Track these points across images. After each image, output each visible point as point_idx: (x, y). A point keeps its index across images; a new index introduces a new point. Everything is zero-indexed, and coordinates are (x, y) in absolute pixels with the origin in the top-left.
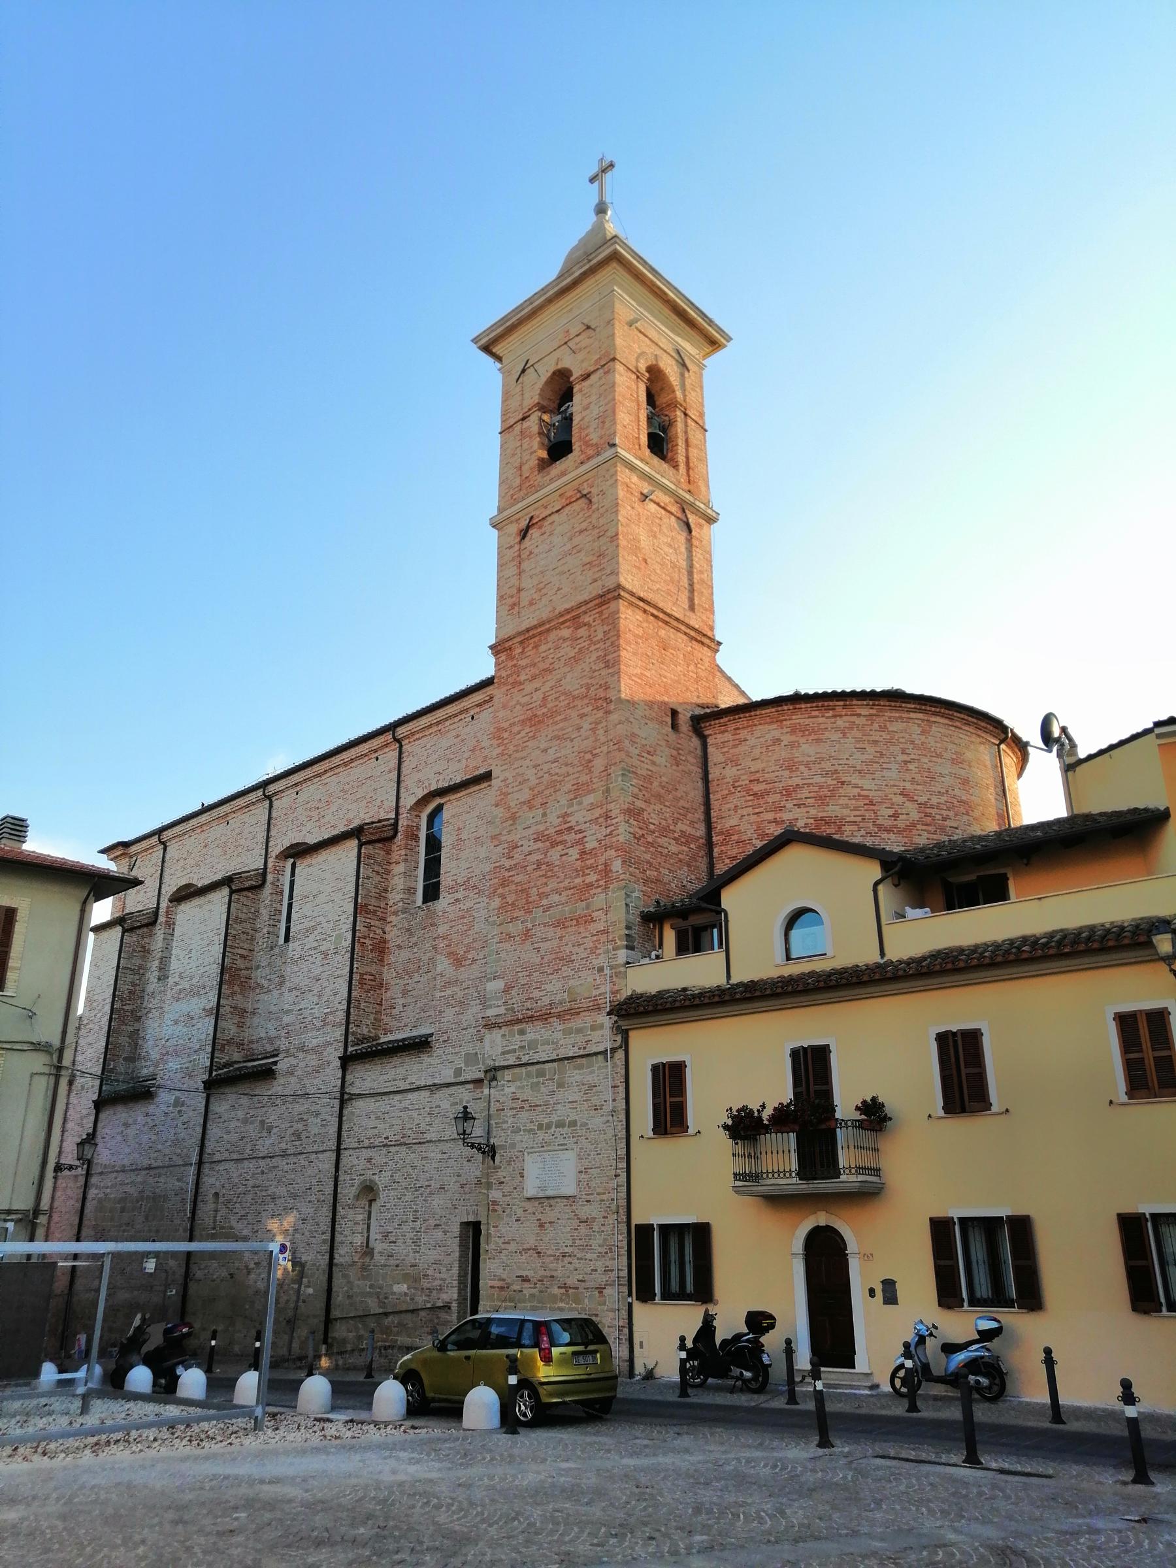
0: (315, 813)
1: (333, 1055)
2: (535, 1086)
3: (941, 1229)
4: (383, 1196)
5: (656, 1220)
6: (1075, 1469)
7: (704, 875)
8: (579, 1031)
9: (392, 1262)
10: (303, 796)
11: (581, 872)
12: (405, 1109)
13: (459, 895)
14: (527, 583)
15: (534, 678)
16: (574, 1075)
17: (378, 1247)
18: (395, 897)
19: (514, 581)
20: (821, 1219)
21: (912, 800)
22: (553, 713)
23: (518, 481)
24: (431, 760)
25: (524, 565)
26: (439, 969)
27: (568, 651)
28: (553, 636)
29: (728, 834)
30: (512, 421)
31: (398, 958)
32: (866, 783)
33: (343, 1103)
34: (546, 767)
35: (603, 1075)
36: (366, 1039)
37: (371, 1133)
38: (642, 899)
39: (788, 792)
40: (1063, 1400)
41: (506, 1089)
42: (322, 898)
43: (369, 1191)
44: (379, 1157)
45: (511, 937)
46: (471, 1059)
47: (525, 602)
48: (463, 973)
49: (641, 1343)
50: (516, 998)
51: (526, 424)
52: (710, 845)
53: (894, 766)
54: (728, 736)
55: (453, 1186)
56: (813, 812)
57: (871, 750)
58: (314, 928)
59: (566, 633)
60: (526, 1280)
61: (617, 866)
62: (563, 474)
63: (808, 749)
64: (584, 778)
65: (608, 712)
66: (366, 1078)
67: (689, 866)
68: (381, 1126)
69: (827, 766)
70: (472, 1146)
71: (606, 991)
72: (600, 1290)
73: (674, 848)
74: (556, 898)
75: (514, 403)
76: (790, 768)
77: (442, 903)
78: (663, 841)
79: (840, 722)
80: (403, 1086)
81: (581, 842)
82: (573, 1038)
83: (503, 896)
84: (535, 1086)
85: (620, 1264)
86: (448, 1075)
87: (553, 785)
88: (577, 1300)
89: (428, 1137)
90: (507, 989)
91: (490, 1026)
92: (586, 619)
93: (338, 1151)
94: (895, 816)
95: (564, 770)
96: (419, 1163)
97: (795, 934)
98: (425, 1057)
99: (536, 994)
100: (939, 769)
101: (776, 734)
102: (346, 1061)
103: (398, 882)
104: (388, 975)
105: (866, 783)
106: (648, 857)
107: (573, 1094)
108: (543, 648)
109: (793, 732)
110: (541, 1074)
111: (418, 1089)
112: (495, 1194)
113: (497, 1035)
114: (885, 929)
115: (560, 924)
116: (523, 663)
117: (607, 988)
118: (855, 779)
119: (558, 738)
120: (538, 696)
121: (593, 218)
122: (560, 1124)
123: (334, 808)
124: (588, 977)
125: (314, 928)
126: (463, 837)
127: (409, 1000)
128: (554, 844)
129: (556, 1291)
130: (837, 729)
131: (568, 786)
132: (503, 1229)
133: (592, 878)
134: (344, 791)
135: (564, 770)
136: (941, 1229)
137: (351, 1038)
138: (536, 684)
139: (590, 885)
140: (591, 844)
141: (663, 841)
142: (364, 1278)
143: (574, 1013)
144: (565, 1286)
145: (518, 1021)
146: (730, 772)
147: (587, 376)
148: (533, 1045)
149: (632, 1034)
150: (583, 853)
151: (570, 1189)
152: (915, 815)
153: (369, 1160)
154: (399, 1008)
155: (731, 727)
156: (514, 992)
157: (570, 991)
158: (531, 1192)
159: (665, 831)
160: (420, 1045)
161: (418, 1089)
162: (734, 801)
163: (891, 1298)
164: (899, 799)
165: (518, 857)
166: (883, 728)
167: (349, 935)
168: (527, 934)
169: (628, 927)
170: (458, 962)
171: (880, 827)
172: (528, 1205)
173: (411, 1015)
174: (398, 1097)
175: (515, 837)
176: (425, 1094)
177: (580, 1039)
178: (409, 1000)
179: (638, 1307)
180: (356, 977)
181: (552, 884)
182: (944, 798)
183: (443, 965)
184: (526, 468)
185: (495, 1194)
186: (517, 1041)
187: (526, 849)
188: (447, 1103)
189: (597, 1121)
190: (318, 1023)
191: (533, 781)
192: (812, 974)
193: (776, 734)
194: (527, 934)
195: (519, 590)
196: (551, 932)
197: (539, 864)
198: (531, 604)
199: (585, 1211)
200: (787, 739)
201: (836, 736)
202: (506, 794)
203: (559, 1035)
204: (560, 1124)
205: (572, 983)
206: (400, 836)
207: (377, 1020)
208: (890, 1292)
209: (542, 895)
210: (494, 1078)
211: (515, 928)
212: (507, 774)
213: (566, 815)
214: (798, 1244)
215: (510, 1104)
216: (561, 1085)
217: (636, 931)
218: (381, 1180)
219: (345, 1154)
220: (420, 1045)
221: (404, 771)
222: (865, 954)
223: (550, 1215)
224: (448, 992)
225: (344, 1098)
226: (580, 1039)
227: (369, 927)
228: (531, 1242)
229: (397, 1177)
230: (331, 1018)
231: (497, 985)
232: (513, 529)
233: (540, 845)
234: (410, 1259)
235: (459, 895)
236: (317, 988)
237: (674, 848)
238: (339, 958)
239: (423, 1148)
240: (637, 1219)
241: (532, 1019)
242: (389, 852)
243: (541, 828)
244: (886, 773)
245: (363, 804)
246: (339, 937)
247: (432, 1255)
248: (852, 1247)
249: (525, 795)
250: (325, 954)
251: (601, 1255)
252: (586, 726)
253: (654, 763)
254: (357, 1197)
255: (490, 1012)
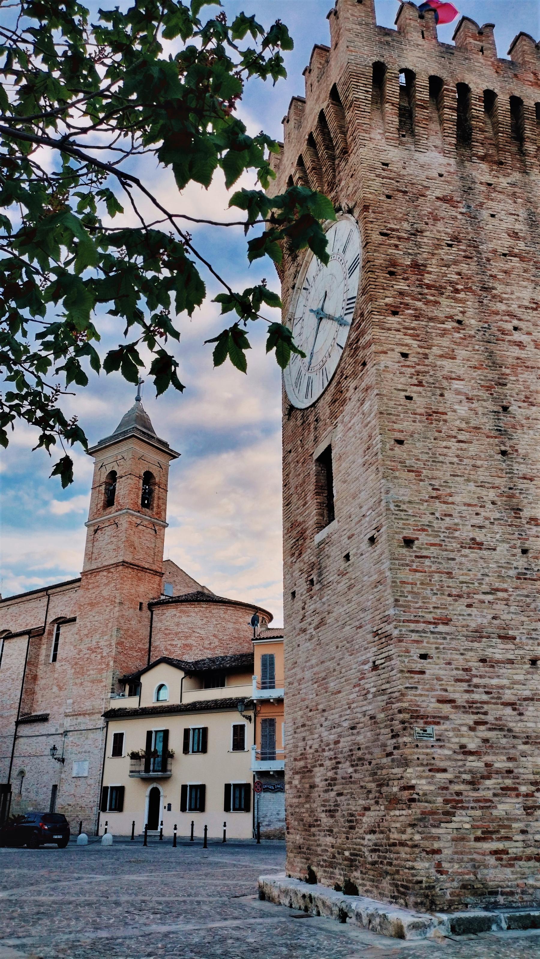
0: (14, 618)
1: (14, 719)
2: (79, 738)
3: (184, 787)
4: (27, 775)
5: (110, 785)
6: (247, 858)
7: (146, 663)
8: (94, 720)
9: (28, 799)
10: (10, 611)
11: (100, 664)
12: (37, 743)
13: (63, 663)
14: (95, 551)
15: (93, 588)
16: (91, 735)
17: (24, 794)
18: (42, 658)
19: (91, 549)
20: (154, 785)
21: (216, 637)
22: (98, 603)
23: (95, 511)
24: (60, 605)
25: (95, 543)
26: (54, 690)
27: (105, 581)
28: (101, 574)
29: (156, 647)
30: (96, 485)
31: (41, 682)
32: (202, 632)
33: (15, 739)
34: (94, 623)
35: (99, 736)
36: (27, 714)
37: (24, 751)
38: (120, 674)
39: (177, 634)
40: (208, 836)
41: (71, 738)
42: (14, 657)
43: (22, 773)
44: (27, 761)
45: (76, 684)
46: (62, 725)
47: (93, 558)
48: (62, 693)
49: (162, 822)
50: (76, 707)
51: (101, 488)
52: (150, 651)
53: (212, 626)
54: (160, 612)
55: (51, 772)
56: (183, 642)
57: (205, 620)
58: (10, 668)
59: (105, 573)
60: (69, 805)
61: (112, 663)
62: (110, 513)
63: (184, 619)
64: (105, 629)
65: (115, 607)
66: (25, 730)
67: (140, 660)
68: (28, 748)
69: (190, 625)
70: (55, 759)
71: (104, 707)
72: (91, 808)
73: (135, 654)
74: (92, 672)
75: (97, 479)
76: (177, 625)
77: (57, 664)
78: (130, 652)
79: (196, 609)
80: (37, 734)
81: (101, 653)
82: (92, 722)
83: (75, 669)
84: (79, 738)
85: (97, 800)
86: (53, 731)
87: (96, 630)
88: (84, 811)
89: (45, 753)
90: (74, 703)
91: (67, 716)
92: (112, 570)
93: (12, 758)
94: (210, 644)
95: (99, 625)
96: (40, 763)
97: (162, 692)
98: (46, 724)
99: (82, 706)
100: (228, 626)
101: (175, 613)
102: (18, 723)
103: (43, 652)
104: (37, 689)
105: (202, 632)
106: (124, 659)
107: (90, 742)
108: (97, 577)
109: (180, 612)
110: (81, 734)
111: (42, 735)
112: (63, 776)
113: (69, 718)
114: (183, 694)
115: (93, 682)
116: (90, 581)
117: (103, 706)
118: (198, 631)
119: (98, 612)
120: (94, 595)
121: (134, 402)
122: (85, 752)
123: (22, 617)
124: (99, 702)
125: (10, 668)
126: (67, 641)
127: (44, 699)
128: (93, 652)
129: (78, 809)
130: (195, 612)
131: (100, 632)
132: (64, 788)
133: (104, 666)
134: (27, 611)
135: (99, 625)
136: (184, 787)
137: (20, 714)
138: (94, 591)
139: (103, 669)
140: (105, 654)
141: (130, 652)
142: (18, 805)
143: (93, 714)
144: (81, 807)
145: (76, 715)
146: (159, 625)
147: (121, 477)
148: (80, 724)
149: (110, 723)
150: (102, 657)
151: (85, 775)
152: (217, 644)
153: (23, 761)
154: (40, 702)
155: (161, 608)
156: (75, 704)
157: (93, 706)
158: (74, 776)
159: (131, 648)
160: (44, 719)
161: (42, 735)
162: (159, 636)
163: (169, 809)
164: (212, 638)
165: (81, 655)
166: (210, 612)
167: (23, 673)
168: (81, 684)
169: (113, 685)
170: (60, 689)
171: (205, 648)
172: (72, 779)
173: (43, 705)
174: (35, 738)
175: (81, 647)
176: (45, 737)
177: (94, 723)
178: (44, 699)
179: (101, 813)
180: (24, 690)
181: (91, 667)
182: (228, 637)
183: (55, 689)
184: (99, 506)
185: (63, 776)
186: (75, 722)
187: (84, 652)
188: (52, 741)
189: (96, 751)
190: (8, 707)
191: (89, 628)
192: (162, 706)
193: (175, 613)
194: (81, 684)
195: (92, 553)
196: (89, 684)
197: (88, 658)
198: (96, 559)
199: (90, 782)
200: (178, 614)
201: (193, 615)
202: (80, 630)
203: (88, 721)
204: (85, 752)
205: (94, 703)
206: (46, 634)
207: (32, 706)
208: (169, 807)
209: (88, 670)
210: (66, 735)
211: (78, 681)
212: (81, 623)
213: (98, 642)
214: (148, 793)
215: (70, 744)
216: (87, 738)
217: (116, 687)
218: (26, 769)
219: (14, 759)
220: (44, 719)
221: (50, 607)
222: (177, 702)
223: (79, 783)
224: (56, 700)
225: (16, 737)
226: (94, 723)
227: (30, 670)
228: (73, 792)
229: (33, 768)
230: (13, 706)
231: (70, 701)
232: (92, 528)
233: (89, 652)
234: (34, 799)
235: (63, 663)
236: (9, 693)
237: (135, 654)
238: (18, 682)
239: (42, 757)
240: (104, 785)
241: (80, 714)
242: (41, 640)
243: (90, 645)
244: (209, 628)
245: (33, 618)
246: (19, 673)
247: (43, 797)
248: (161, 794)
249: (86, 632)
250: (13, 680)
251: (93, 797)
252: (108, 610)
253: (130, 624)
254: (18, 775)
255: (67, 711)
